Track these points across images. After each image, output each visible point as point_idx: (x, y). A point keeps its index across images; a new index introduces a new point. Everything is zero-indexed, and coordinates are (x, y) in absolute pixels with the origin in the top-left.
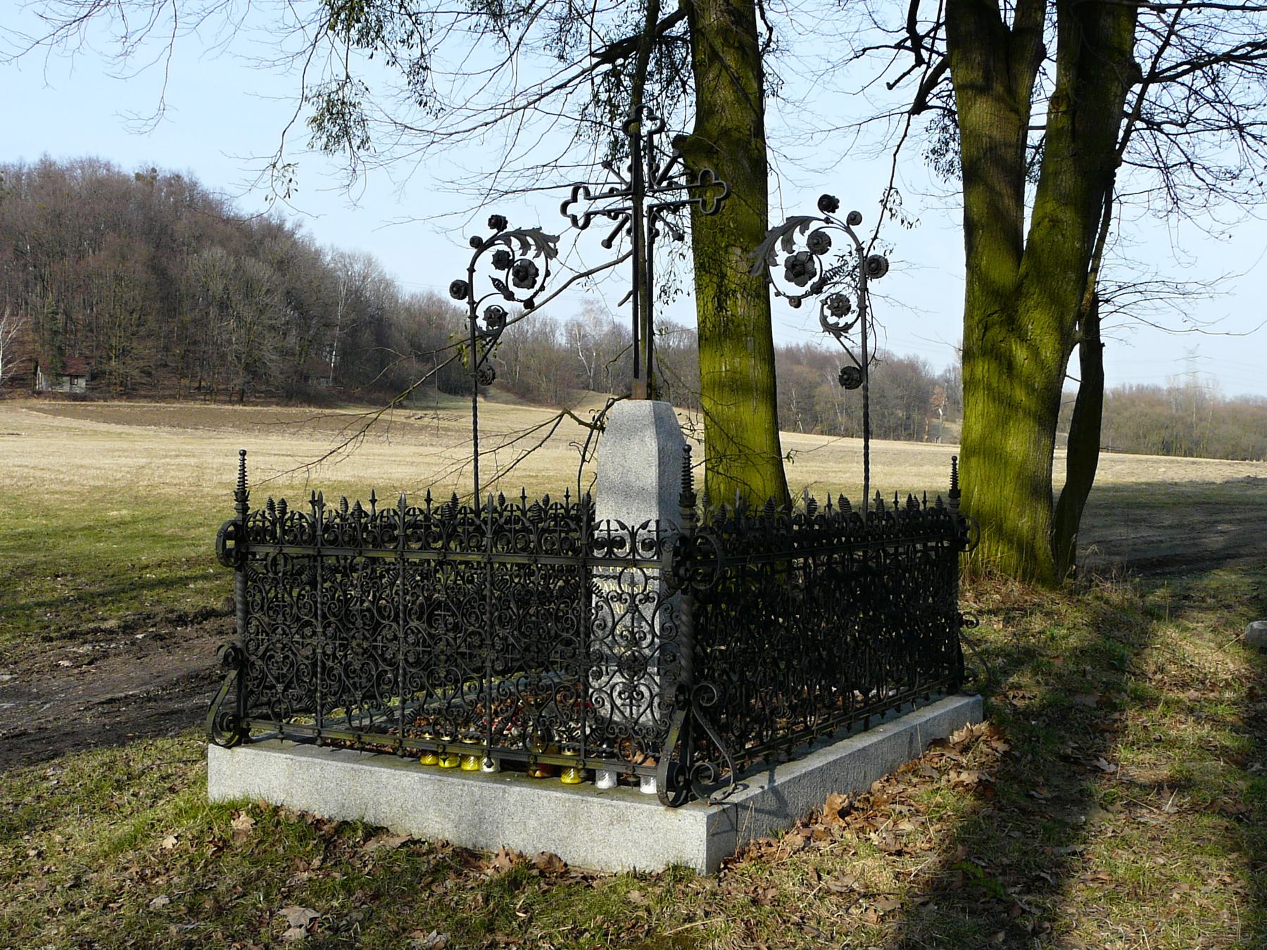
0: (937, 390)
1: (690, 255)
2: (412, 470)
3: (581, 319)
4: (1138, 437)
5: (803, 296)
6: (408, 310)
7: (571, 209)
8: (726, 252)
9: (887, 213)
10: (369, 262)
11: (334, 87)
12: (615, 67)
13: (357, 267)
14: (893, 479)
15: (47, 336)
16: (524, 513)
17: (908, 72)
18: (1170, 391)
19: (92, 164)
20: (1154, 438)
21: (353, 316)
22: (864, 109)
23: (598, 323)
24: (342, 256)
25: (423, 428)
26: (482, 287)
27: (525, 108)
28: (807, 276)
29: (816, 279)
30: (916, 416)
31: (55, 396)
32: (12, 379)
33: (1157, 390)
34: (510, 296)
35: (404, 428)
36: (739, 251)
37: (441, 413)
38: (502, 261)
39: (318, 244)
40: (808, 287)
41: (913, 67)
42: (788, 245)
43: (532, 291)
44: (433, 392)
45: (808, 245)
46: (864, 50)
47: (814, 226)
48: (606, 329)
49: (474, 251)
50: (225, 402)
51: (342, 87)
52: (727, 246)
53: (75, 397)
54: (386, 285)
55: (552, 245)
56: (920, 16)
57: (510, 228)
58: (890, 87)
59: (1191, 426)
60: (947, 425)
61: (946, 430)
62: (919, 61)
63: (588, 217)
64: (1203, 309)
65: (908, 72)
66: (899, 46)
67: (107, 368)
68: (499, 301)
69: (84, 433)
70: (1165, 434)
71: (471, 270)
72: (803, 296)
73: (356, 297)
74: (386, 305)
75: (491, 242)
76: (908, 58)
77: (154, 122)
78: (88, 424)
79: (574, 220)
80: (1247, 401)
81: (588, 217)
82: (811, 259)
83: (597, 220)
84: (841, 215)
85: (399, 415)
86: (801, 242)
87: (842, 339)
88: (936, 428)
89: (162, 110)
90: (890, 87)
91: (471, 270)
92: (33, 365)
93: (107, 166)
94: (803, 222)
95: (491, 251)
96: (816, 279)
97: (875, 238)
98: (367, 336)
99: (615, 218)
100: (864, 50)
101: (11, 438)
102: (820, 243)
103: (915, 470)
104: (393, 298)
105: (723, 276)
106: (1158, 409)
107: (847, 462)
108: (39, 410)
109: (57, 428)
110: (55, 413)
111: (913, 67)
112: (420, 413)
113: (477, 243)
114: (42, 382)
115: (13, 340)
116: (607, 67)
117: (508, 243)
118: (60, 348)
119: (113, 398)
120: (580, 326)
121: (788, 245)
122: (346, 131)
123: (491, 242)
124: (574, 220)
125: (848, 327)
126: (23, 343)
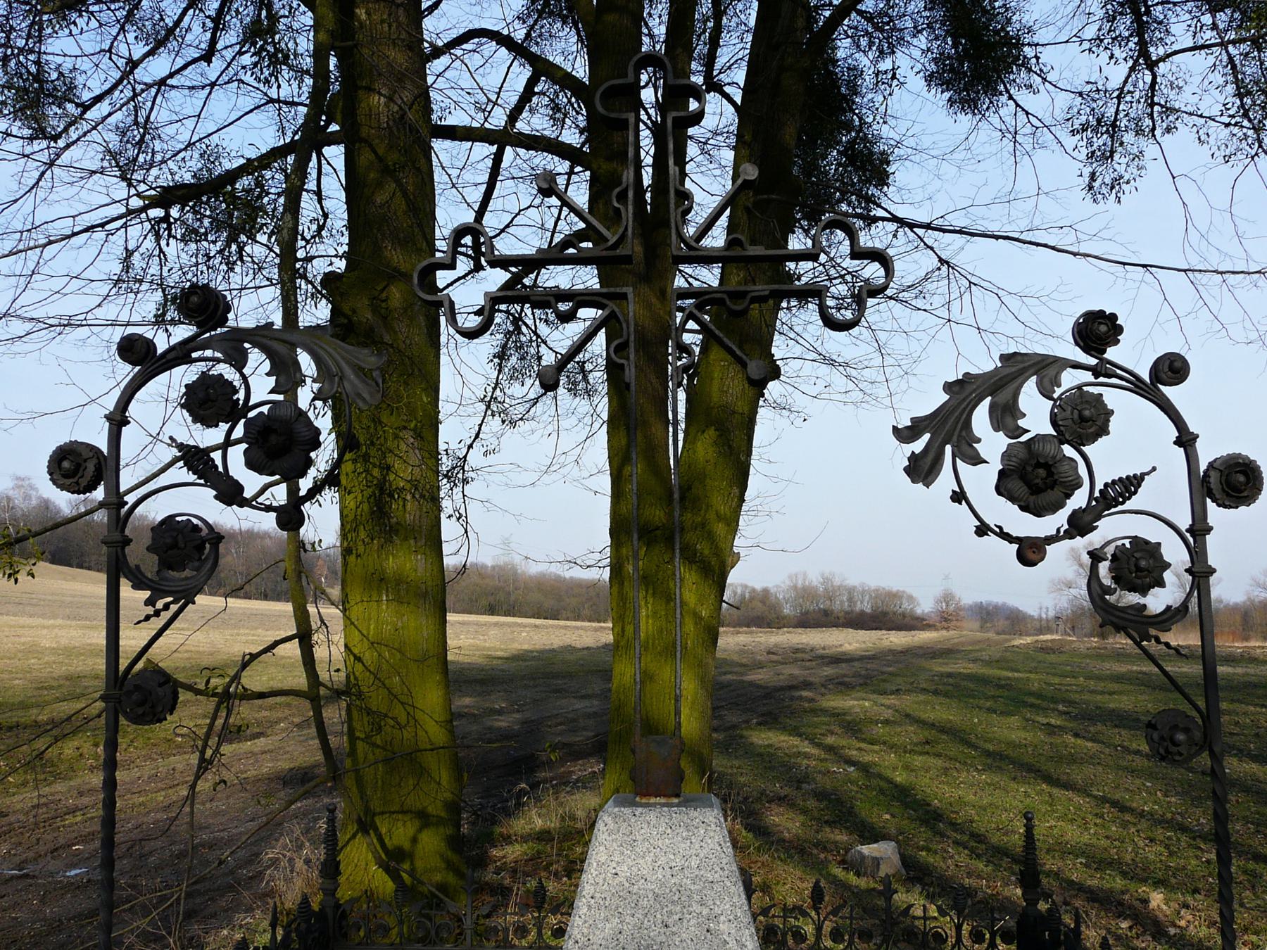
0: (320, 562)
3: (11, 493)
4: (471, 600)
9: (489, 412)
12: (168, 215)
18: (493, 567)
20: (484, 602)
23: (27, 497)
26: (140, 456)
27: (45, 246)
28: (1056, 493)
33: (484, 566)
34: (231, 493)
38: (208, 402)
40: (1060, 519)
42: (1006, 417)
47: (1070, 379)
48: (34, 502)
49: (126, 371)
59: (509, 593)
68: (199, 503)
70: (491, 599)
71: (118, 420)
75: (180, 354)
80: (544, 575)
84: (1133, 353)
86: (1036, 414)
91: (118, 420)
94: (1048, 368)
95: (184, 375)
97: (477, 436)
102: (1082, 420)
106: (487, 581)
113: (135, 350)
116: (156, 213)
117: (239, 362)
120: (9, 499)
121: (1006, 417)
123: (180, 354)
125: (1171, 616)
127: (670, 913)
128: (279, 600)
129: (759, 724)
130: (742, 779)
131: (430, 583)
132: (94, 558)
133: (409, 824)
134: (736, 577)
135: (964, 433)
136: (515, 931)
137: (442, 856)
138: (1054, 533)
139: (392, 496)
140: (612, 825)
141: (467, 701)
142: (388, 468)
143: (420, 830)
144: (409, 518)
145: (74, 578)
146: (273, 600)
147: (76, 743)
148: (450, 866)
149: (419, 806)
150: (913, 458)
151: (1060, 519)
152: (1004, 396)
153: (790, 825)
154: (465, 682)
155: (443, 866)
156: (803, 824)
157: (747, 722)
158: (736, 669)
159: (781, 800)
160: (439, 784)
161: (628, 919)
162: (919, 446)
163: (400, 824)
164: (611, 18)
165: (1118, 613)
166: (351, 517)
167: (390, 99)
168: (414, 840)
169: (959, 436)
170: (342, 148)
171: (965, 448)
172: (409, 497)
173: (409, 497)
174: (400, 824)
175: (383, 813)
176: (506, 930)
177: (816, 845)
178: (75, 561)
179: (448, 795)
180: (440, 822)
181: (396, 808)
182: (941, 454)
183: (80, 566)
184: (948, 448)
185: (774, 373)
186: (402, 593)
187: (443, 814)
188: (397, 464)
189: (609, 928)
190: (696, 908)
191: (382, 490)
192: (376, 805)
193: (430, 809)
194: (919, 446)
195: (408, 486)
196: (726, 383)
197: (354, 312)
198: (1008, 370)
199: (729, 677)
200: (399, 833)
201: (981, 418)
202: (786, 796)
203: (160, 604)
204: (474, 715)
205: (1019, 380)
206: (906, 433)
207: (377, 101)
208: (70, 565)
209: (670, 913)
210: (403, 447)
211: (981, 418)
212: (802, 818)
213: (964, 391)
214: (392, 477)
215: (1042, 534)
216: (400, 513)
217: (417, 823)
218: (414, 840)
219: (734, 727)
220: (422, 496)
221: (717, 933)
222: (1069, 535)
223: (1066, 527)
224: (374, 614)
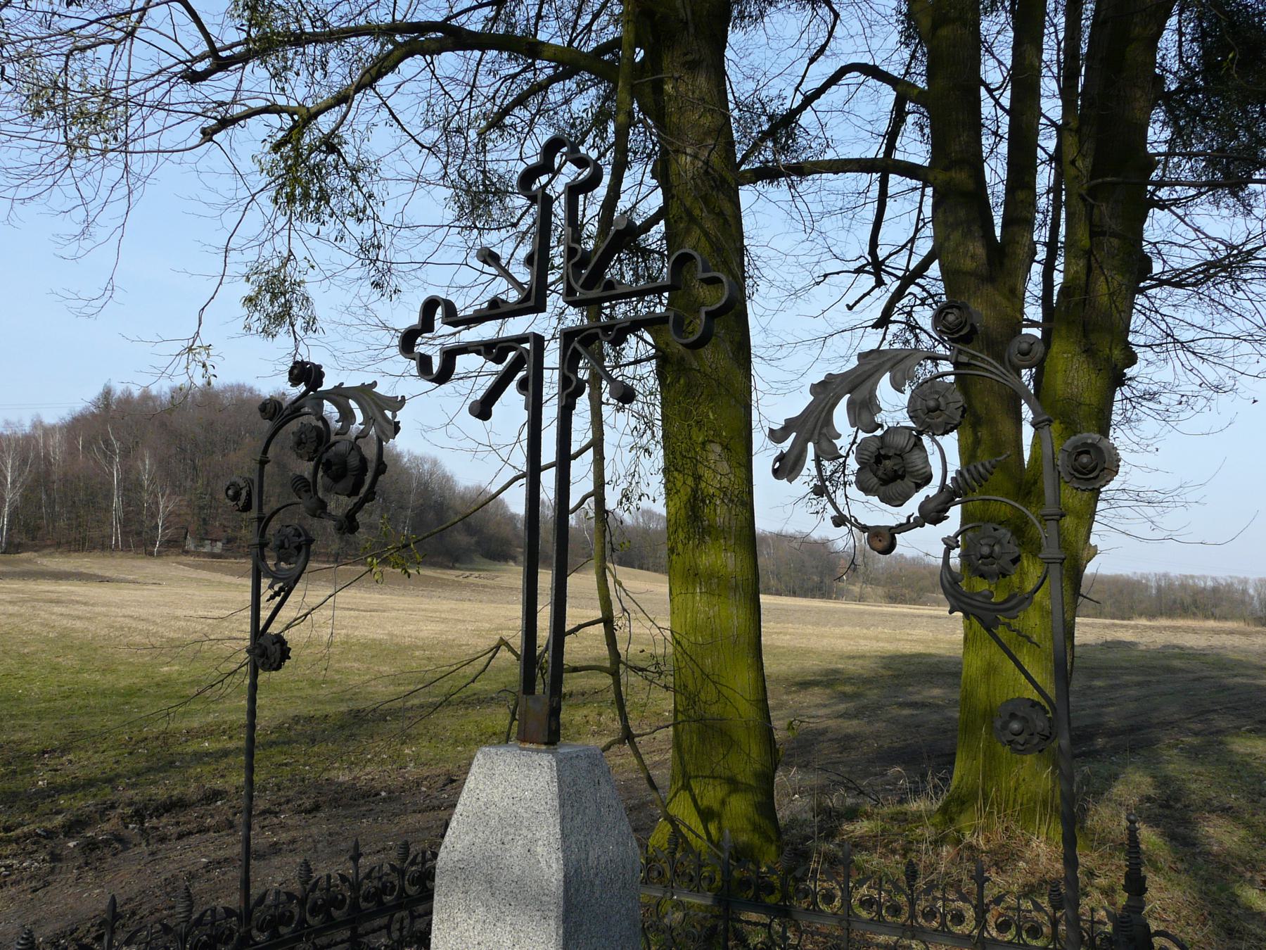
0: (842, 562)
1: (659, 453)
2: (442, 627)
5: (903, 528)
6: (462, 498)
7: (423, 346)
8: (703, 448)
10: (435, 463)
11: (276, 263)
13: (426, 467)
14: (825, 642)
15: (196, 511)
16: (356, 886)
17: (868, 293)
19: (240, 388)
21: (421, 501)
22: (822, 327)
24: (416, 458)
25: (468, 585)
28: (909, 482)
29: (931, 490)
30: (827, 581)
31: (198, 555)
32: (168, 541)
35: (443, 584)
36: (718, 449)
37: (483, 574)
39: (398, 449)
40: (912, 506)
41: (873, 289)
42: (864, 410)
43: (355, 499)
44: (477, 558)
45: (913, 413)
46: (826, 276)
49: (267, 425)
50: (324, 562)
51: (284, 265)
52: (704, 444)
53: (213, 555)
54: (447, 480)
55: (389, 414)
56: (881, 239)
57: (328, 384)
58: (850, 308)
60: (851, 587)
61: (848, 590)
62: (880, 283)
63: (449, 356)
64: (1171, 520)
65: (868, 293)
66: (859, 271)
67: (239, 535)
69: (210, 583)
72: (903, 528)
73: (425, 488)
74: (447, 494)
76: (868, 281)
77: (100, 303)
78: (217, 577)
79: (424, 362)
81: (449, 356)
82: (918, 444)
83: (465, 363)
85: (451, 575)
87: (1001, 632)
88: (842, 589)
89: (110, 287)
90: (850, 308)
92: (184, 531)
93: (251, 390)
96: (931, 490)
98: (431, 515)
99: (498, 360)
100: (826, 276)
101: (154, 587)
103: (837, 630)
104: (452, 489)
105: (698, 478)
107: (783, 622)
108: (185, 565)
109: (192, 579)
110: (197, 567)
111: (873, 289)
112: (468, 573)
114: (190, 544)
115: (171, 513)
118: (204, 519)
119: (242, 557)
122: (287, 307)
124: (424, 362)
126: (179, 515)
127: (507, 833)
128: (805, 596)
129: (1250, 731)
130: (1194, 786)
131: (739, 578)
132: (651, 560)
133: (718, 788)
134: (1090, 569)
135: (825, 431)
136: (824, 896)
137: (749, 820)
138: (904, 521)
139: (703, 501)
140: (482, 761)
141: (936, 692)
142: (700, 477)
143: (730, 794)
144: (719, 521)
145: (636, 578)
146: (799, 596)
147: (585, 712)
148: (756, 828)
149: (728, 773)
150: (781, 458)
151: (912, 506)
152: (862, 393)
153: (1225, 838)
154: (938, 674)
155: (750, 827)
156: (1242, 839)
157: (1239, 728)
158: (1250, 672)
159: (1226, 811)
160: (748, 755)
161: (480, 834)
162: (786, 445)
163: (710, 788)
164: (944, 32)
165: (966, 600)
166: (673, 521)
167: (695, 157)
168: (723, 803)
169: (820, 433)
170: (891, 176)
171: (825, 444)
172: (718, 502)
173: (718, 502)
174: (710, 788)
175: (696, 777)
176: (815, 894)
177: (1245, 863)
178: (637, 563)
179: (758, 766)
180: (748, 788)
181: (708, 773)
182: (803, 451)
183: (642, 568)
184: (811, 446)
185: (1132, 359)
186: (714, 586)
187: (752, 782)
188: (707, 474)
189: (468, 839)
190: (524, 832)
191: (695, 498)
192: (691, 769)
193: (739, 777)
194: (786, 445)
195: (717, 493)
196: (1072, 372)
197: (667, 344)
198: (867, 367)
199: (1239, 680)
200: (711, 795)
201: (840, 415)
202: (1231, 808)
203: (276, 588)
204: (938, 706)
205: (877, 375)
206: (778, 435)
207: (685, 160)
208: (633, 567)
209: (507, 833)
210: (712, 457)
211: (840, 415)
212: (1242, 833)
213: (826, 391)
214: (703, 485)
215: (893, 523)
216: (712, 517)
217: (726, 787)
218: (723, 803)
219: (1219, 732)
220: (731, 501)
221: (535, 855)
222: (919, 523)
223: (917, 514)
224: (690, 604)
